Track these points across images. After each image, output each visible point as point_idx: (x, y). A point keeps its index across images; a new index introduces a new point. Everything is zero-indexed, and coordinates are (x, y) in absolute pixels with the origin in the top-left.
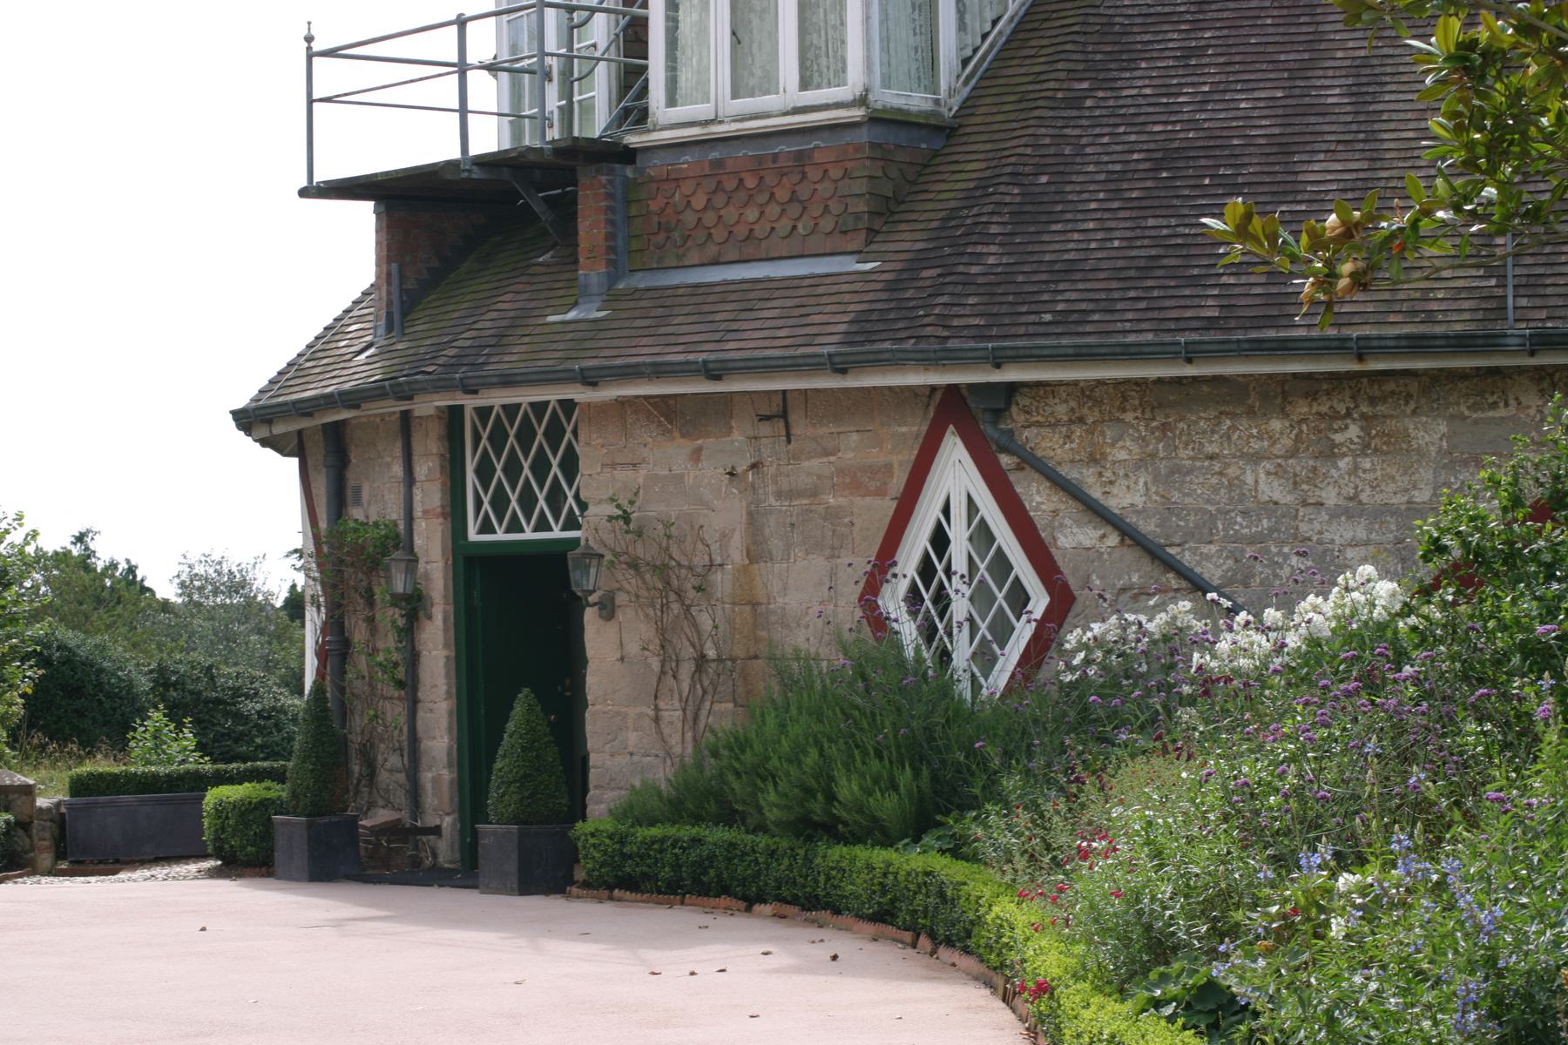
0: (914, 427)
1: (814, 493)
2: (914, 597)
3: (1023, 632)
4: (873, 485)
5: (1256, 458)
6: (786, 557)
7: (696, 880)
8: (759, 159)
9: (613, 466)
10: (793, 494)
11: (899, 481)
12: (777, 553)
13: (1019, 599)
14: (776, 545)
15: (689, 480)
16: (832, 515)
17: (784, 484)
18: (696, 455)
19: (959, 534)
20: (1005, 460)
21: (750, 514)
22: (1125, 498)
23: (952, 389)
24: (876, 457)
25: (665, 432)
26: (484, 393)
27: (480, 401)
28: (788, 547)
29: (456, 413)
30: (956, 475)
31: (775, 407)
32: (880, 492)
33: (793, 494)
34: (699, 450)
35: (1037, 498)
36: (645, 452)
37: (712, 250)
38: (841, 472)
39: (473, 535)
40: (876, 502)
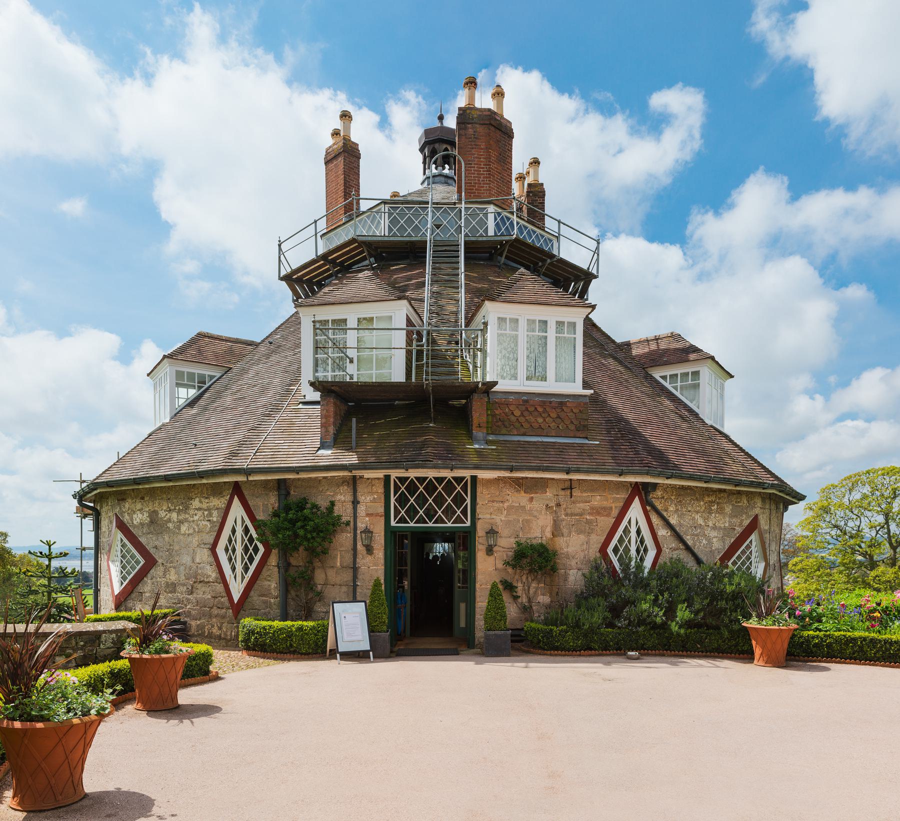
0: (623, 495)
1: (581, 515)
2: (646, 550)
3: (257, 559)
4: (605, 513)
5: (697, 512)
6: (569, 535)
7: (246, 641)
8: (544, 402)
9: (493, 501)
10: (572, 515)
11: (615, 513)
12: (565, 534)
13: (256, 550)
14: (565, 531)
15: (528, 508)
16: (589, 522)
17: (569, 511)
18: (531, 499)
19: (633, 530)
20: (648, 508)
21: (554, 521)
22: (673, 521)
23: (236, 482)
24: (605, 504)
25: (518, 491)
26: (456, 471)
27: (401, 473)
28: (570, 532)
29: (387, 478)
30: (636, 512)
31: (567, 484)
32: (608, 515)
33: (572, 515)
34: (532, 498)
35: (655, 519)
36: (508, 497)
37: (522, 430)
38: (592, 508)
39: (393, 523)
40: (606, 519)
